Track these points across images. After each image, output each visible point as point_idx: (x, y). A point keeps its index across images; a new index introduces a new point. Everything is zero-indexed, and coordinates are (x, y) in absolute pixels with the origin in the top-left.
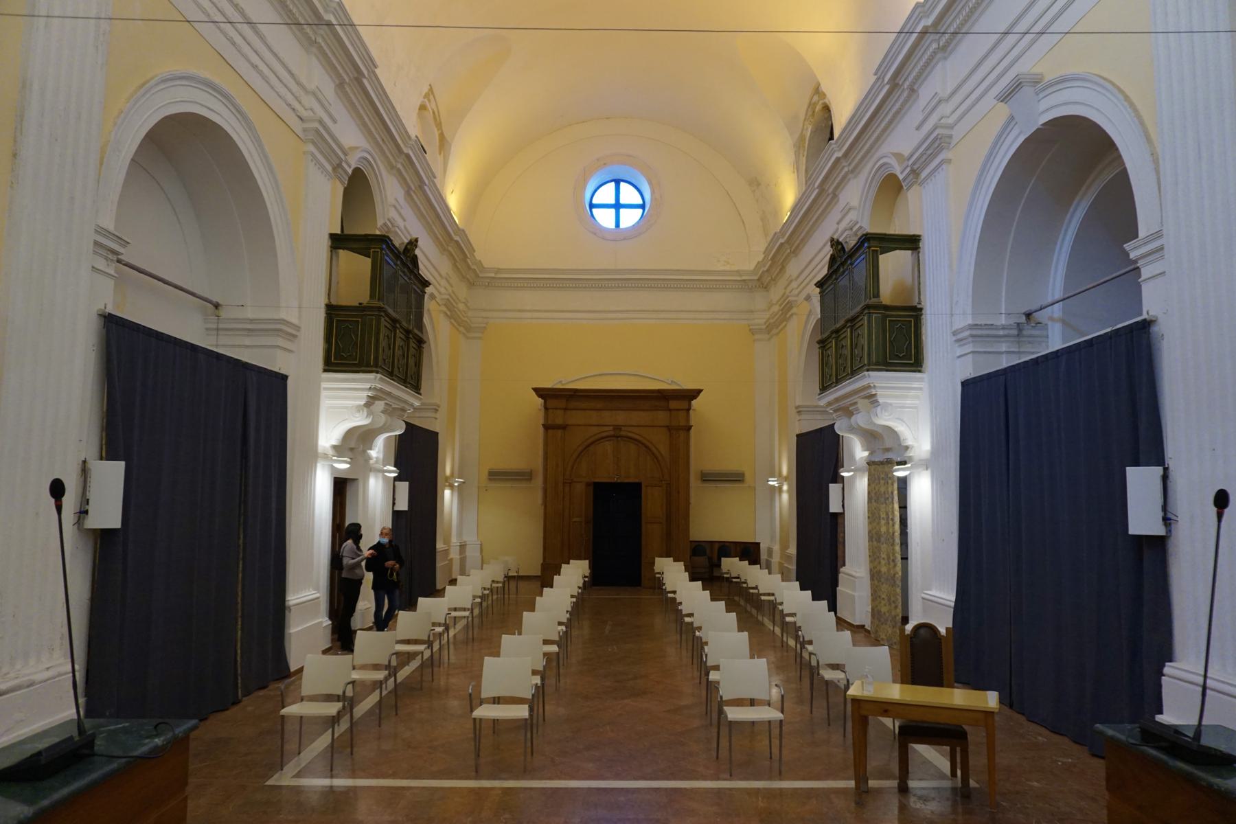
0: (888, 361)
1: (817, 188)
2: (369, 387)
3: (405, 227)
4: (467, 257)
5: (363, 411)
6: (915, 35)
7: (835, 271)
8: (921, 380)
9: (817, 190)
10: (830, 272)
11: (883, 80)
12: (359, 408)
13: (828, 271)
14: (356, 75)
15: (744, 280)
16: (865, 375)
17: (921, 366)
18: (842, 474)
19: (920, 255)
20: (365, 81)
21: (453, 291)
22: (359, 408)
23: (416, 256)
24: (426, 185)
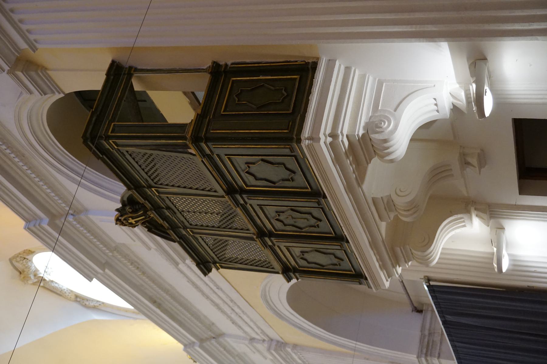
0: (281, 101)
1: (103, 270)
7: (174, 227)
8: (331, 64)
9: (107, 270)
10: (174, 236)
11: (100, 273)
16: (308, 147)
17: (307, 64)
19: (139, 67)
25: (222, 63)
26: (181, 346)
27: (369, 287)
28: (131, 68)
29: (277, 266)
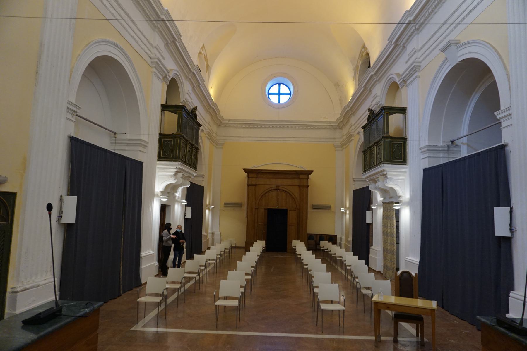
2: (176, 167)
3: (192, 102)
4: (217, 115)
5: (173, 177)
6: (404, 25)
7: (370, 122)
10: (368, 122)
12: (171, 176)
13: (367, 122)
14: (173, 40)
15: (332, 125)
16: (382, 166)
17: (406, 162)
18: (372, 207)
19: (406, 116)
20: (177, 42)
21: (192, 102)
22: (171, 176)
23: (196, 114)
24: (177, 41)
25: (407, 140)
26: (409, 9)
27: (363, 174)
28: (406, 113)
29: (365, 149)
